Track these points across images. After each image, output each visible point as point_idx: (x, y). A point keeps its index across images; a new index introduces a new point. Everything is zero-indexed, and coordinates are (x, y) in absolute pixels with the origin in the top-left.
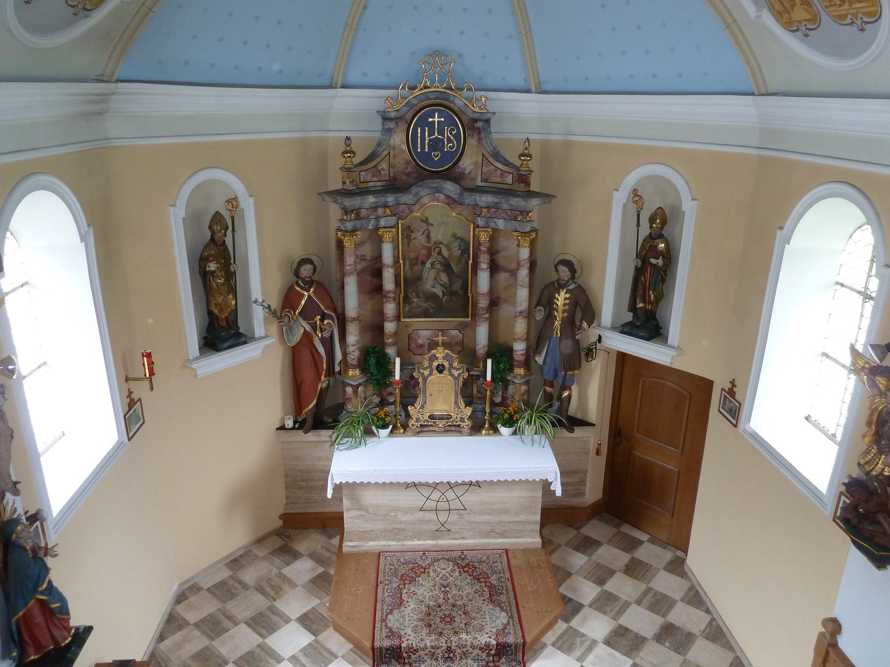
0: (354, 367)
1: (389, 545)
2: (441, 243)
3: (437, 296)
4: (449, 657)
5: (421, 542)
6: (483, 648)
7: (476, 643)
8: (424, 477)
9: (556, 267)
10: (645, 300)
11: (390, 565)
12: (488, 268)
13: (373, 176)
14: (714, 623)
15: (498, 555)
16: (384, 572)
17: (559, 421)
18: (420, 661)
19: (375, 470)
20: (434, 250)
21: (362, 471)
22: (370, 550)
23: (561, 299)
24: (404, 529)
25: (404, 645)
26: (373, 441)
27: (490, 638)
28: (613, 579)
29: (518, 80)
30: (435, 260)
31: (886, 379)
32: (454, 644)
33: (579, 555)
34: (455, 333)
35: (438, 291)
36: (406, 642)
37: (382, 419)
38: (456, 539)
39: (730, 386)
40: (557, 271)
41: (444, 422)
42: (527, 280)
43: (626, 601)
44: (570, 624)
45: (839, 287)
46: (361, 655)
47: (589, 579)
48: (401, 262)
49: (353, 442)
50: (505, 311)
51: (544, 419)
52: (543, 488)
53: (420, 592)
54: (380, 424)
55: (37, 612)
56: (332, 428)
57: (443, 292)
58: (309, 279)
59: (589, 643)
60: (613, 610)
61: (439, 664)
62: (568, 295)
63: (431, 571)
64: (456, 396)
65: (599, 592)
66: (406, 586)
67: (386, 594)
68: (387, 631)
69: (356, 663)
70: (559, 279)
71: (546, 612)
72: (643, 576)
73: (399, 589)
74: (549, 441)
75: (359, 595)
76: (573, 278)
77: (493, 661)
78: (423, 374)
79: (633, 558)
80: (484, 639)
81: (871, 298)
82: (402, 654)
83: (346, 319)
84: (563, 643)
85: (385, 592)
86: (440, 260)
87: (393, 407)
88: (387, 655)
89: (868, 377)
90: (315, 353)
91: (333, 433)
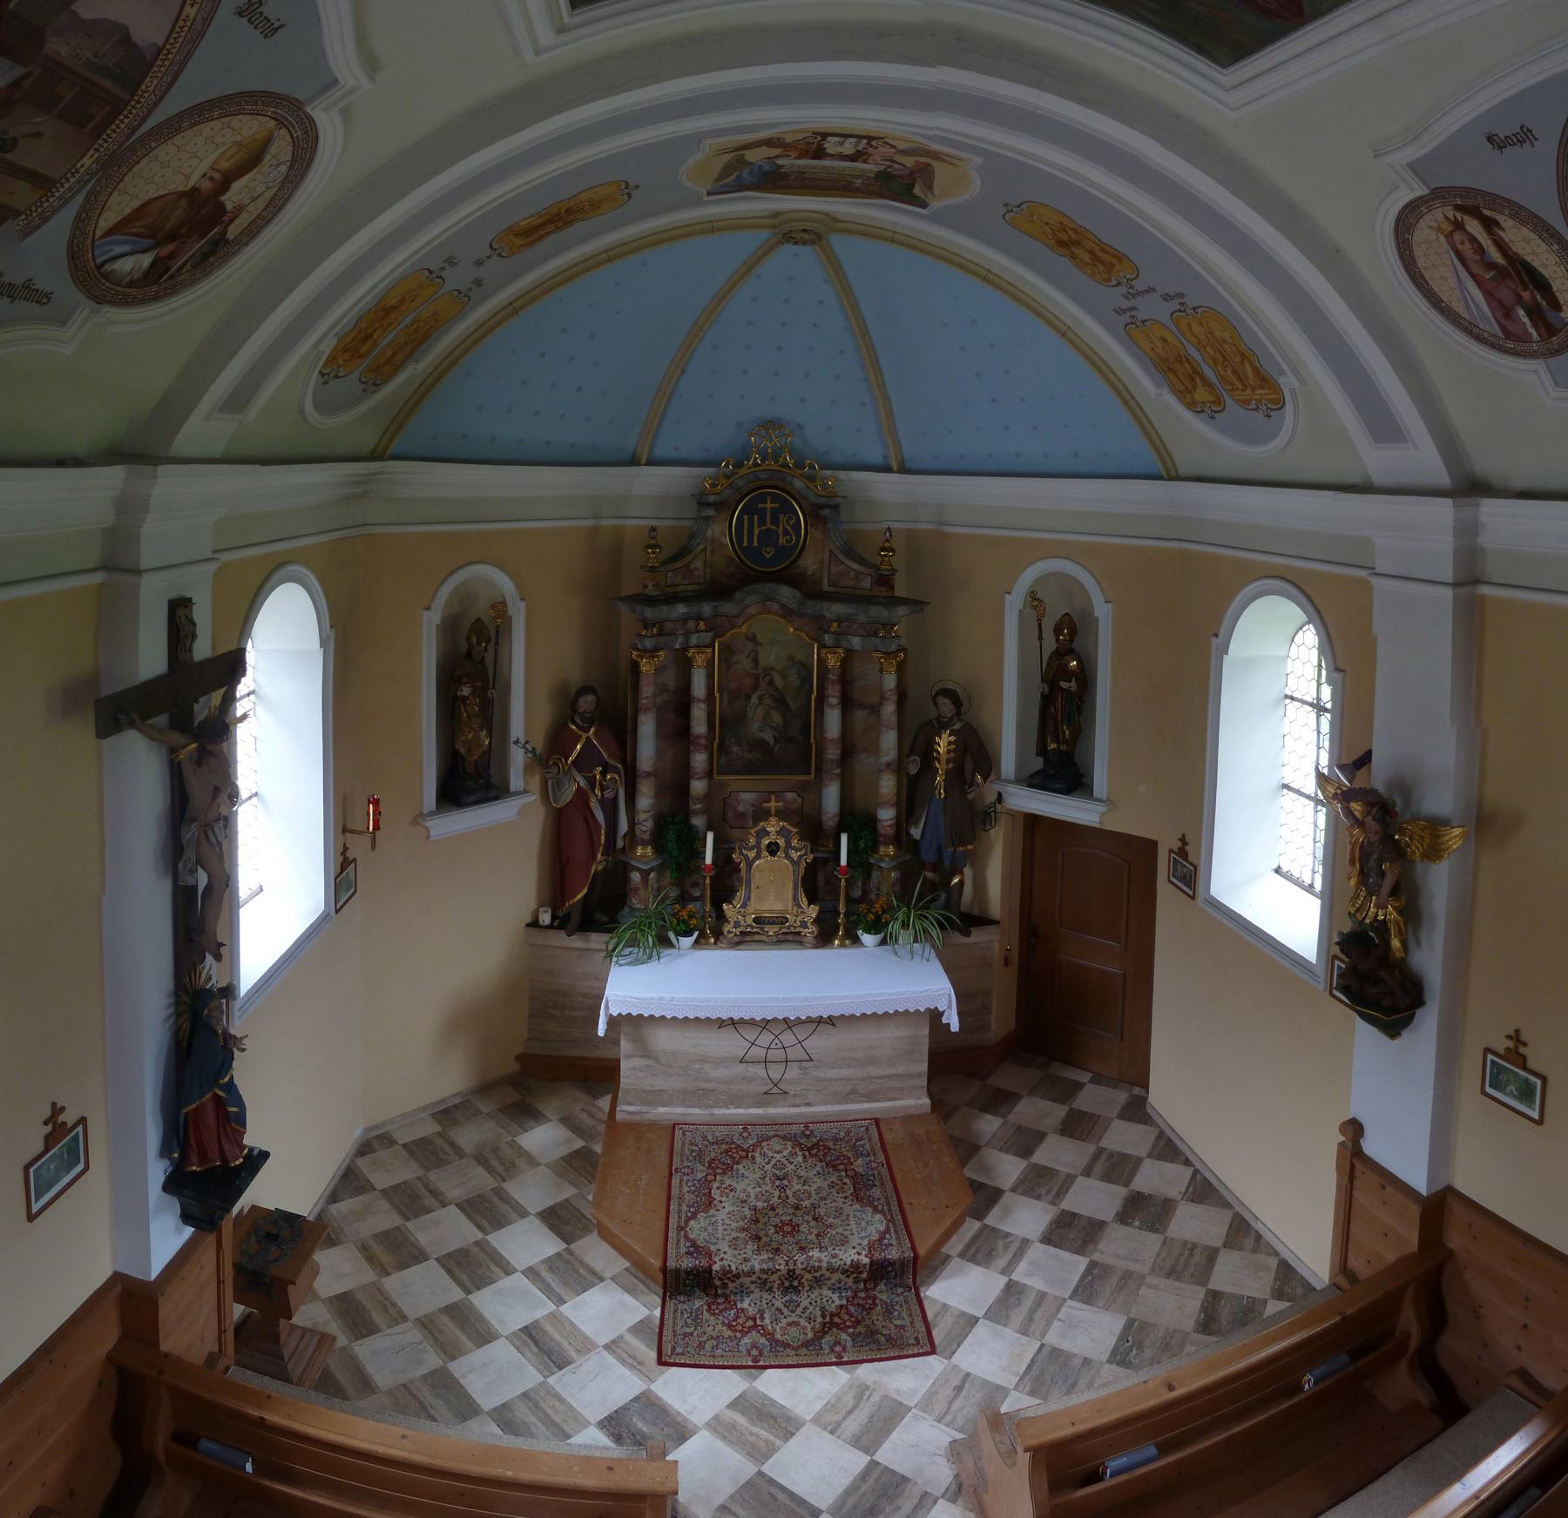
0: (645, 844)
1: (689, 1114)
2: (773, 669)
4: (791, 1286)
5: (741, 1111)
7: (836, 1263)
9: (934, 699)
10: (1058, 739)
11: (692, 1144)
14: (1198, 1176)
15: (864, 1129)
16: (682, 1155)
17: (948, 919)
18: (742, 1292)
19: (673, 998)
21: (653, 999)
23: (943, 743)
24: (714, 1090)
25: (716, 1267)
26: (669, 955)
27: (859, 1254)
28: (1043, 1145)
29: (875, 456)
30: (764, 692)
31: (1360, 803)
32: (800, 1266)
33: (989, 1117)
34: (790, 796)
35: (768, 736)
36: (719, 1263)
37: (684, 922)
38: (796, 1106)
39: (1180, 844)
40: (936, 704)
41: (776, 928)
42: (894, 719)
43: (1068, 1174)
44: (984, 1222)
45: (1288, 701)
46: (644, 1279)
47: (1007, 1152)
48: (717, 695)
49: (641, 954)
50: (863, 763)
51: (926, 918)
52: (930, 1022)
53: (740, 1187)
54: (681, 929)
55: (210, 1111)
56: (610, 931)
57: (775, 738)
58: (589, 715)
59: (1017, 1244)
60: (1051, 1191)
61: (774, 1297)
62: (952, 738)
63: (757, 1155)
64: (795, 889)
65: (1025, 1168)
66: (718, 1177)
67: (686, 1189)
68: (688, 1244)
69: (635, 1290)
70: (939, 716)
71: (947, 1207)
72: (1090, 1133)
73: (706, 1182)
74: (936, 952)
75: (642, 1187)
76: (958, 713)
77: (866, 1289)
79: (1071, 1109)
80: (848, 1256)
81: (1326, 710)
83: (638, 773)
84: (977, 1251)
85: (684, 1185)
87: (698, 904)
88: (687, 1281)
89: (1342, 804)
90: (590, 819)
91: (611, 938)
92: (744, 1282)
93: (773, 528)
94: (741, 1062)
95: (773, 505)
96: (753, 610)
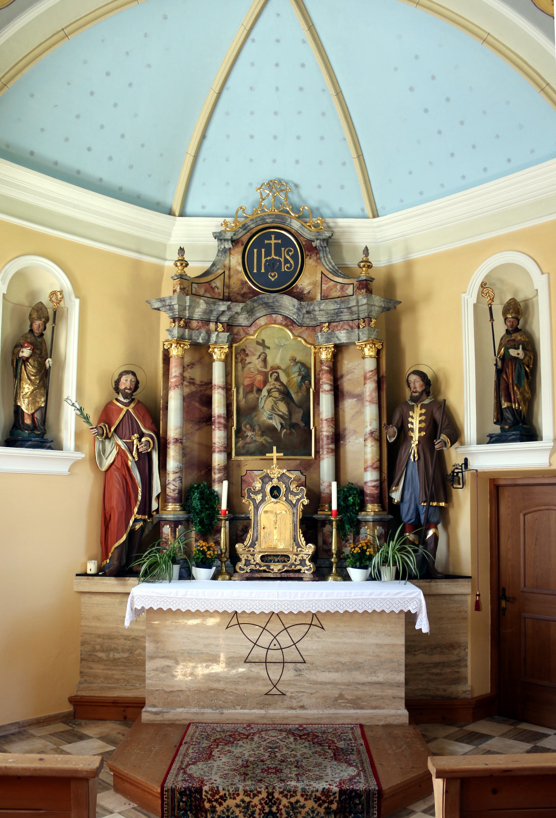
2: (279, 368)
3: (274, 429)
6: (319, 799)
7: (310, 789)
8: (249, 604)
12: (331, 390)
13: (205, 291)
20: (271, 376)
22: (178, 720)
24: (223, 690)
30: (272, 387)
35: (276, 423)
38: (292, 708)
57: (281, 424)
62: (423, 411)
64: (295, 530)
78: (254, 500)
82: (203, 802)
86: (277, 387)
88: (181, 804)
92: (229, 805)
93: (277, 258)
94: (245, 662)
95: (276, 241)
96: (262, 321)
